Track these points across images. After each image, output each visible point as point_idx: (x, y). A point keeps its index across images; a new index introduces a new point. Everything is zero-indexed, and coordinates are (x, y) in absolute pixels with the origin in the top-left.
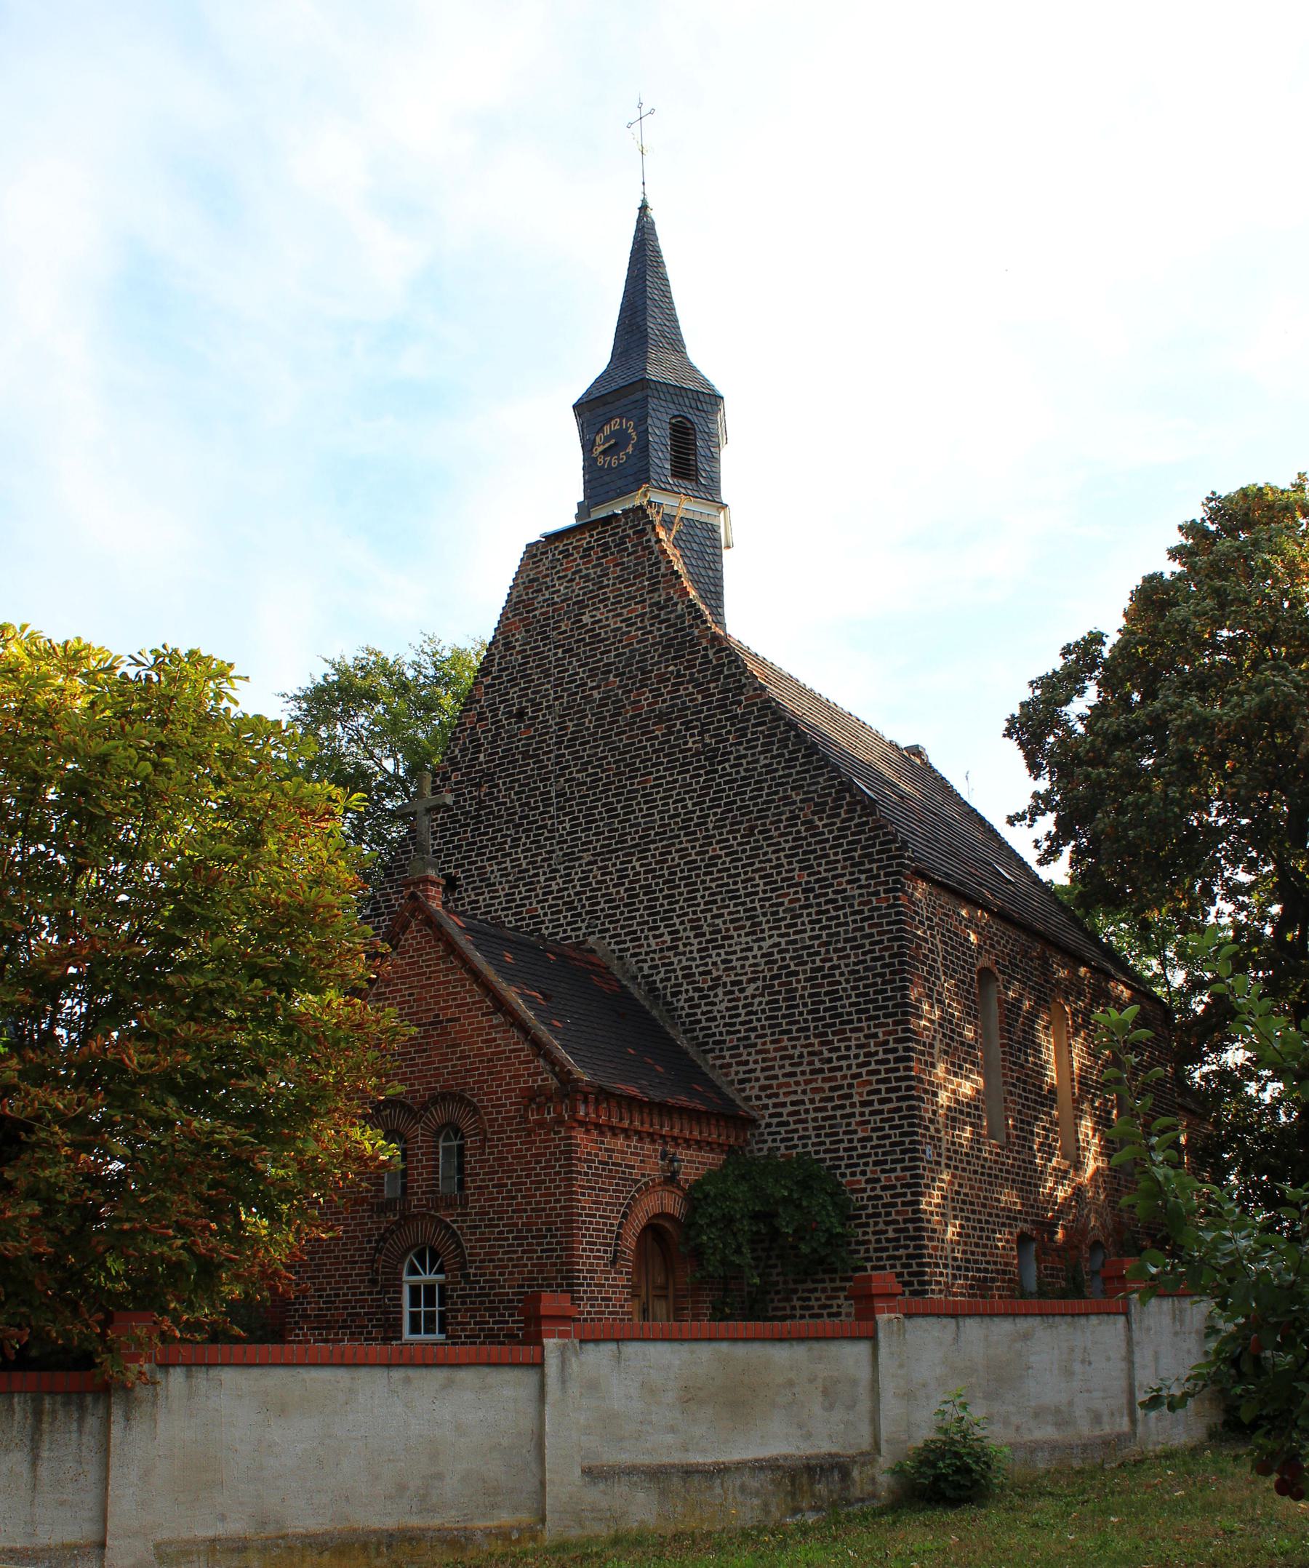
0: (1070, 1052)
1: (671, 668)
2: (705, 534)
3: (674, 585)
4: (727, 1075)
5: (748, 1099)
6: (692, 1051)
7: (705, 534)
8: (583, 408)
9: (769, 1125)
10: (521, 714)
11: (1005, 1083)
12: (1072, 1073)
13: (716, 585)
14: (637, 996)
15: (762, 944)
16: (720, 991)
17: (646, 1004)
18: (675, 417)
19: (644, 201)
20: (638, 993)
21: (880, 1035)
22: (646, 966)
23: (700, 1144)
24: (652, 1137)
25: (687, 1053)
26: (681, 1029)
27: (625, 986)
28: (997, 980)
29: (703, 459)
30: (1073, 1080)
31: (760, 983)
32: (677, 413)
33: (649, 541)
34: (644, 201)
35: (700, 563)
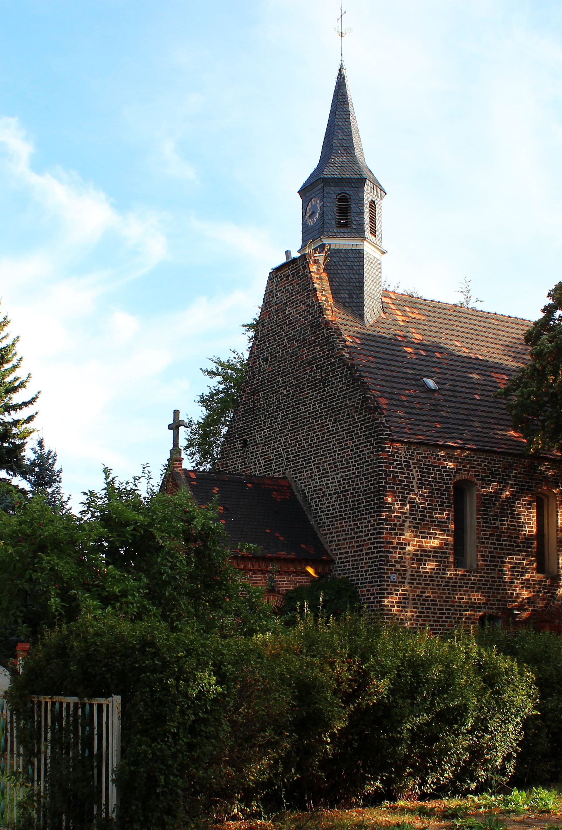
0: (557, 515)
1: (313, 338)
2: (354, 255)
3: (314, 296)
4: (326, 538)
5: (332, 550)
6: (316, 527)
7: (354, 255)
8: (304, 192)
9: (338, 563)
10: (267, 360)
11: (478, 538)
12: (557, 526)
13: (359, 282)
14: (300, 500)
15: (338, 476)
16: (325, 498)
17: (302, 503)
18: (339, 194)
19: (341, 66)
20: (300, 498)
21: (372, 521)
22: (303, 485)
23: (289, 573)
24: (263, 572)
25: (313, 528)
26: (313, 516)
27: (295, 495)
28: (476, 484)
29: (355, 214)
30: (557, 531)
31: (337, 495)
32: (340, 192)
33: (307, 272)
34: (341, 66)
35: (351, 272)
